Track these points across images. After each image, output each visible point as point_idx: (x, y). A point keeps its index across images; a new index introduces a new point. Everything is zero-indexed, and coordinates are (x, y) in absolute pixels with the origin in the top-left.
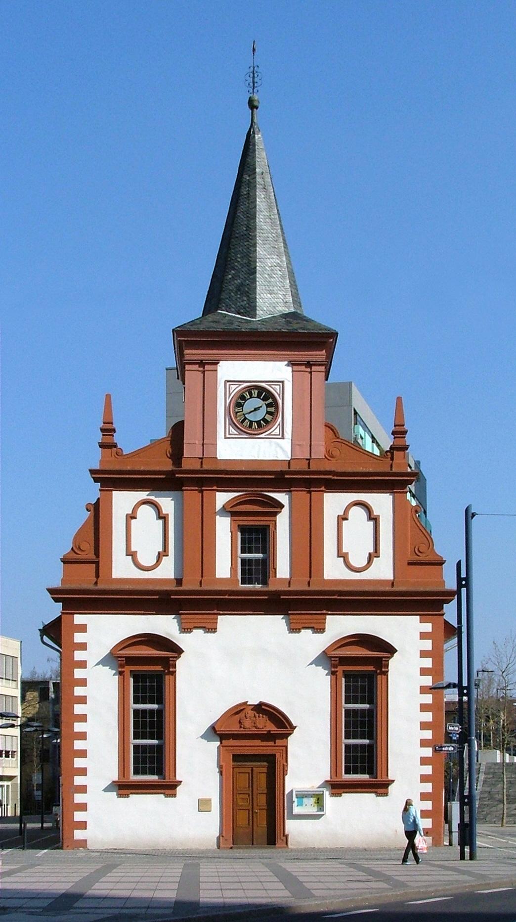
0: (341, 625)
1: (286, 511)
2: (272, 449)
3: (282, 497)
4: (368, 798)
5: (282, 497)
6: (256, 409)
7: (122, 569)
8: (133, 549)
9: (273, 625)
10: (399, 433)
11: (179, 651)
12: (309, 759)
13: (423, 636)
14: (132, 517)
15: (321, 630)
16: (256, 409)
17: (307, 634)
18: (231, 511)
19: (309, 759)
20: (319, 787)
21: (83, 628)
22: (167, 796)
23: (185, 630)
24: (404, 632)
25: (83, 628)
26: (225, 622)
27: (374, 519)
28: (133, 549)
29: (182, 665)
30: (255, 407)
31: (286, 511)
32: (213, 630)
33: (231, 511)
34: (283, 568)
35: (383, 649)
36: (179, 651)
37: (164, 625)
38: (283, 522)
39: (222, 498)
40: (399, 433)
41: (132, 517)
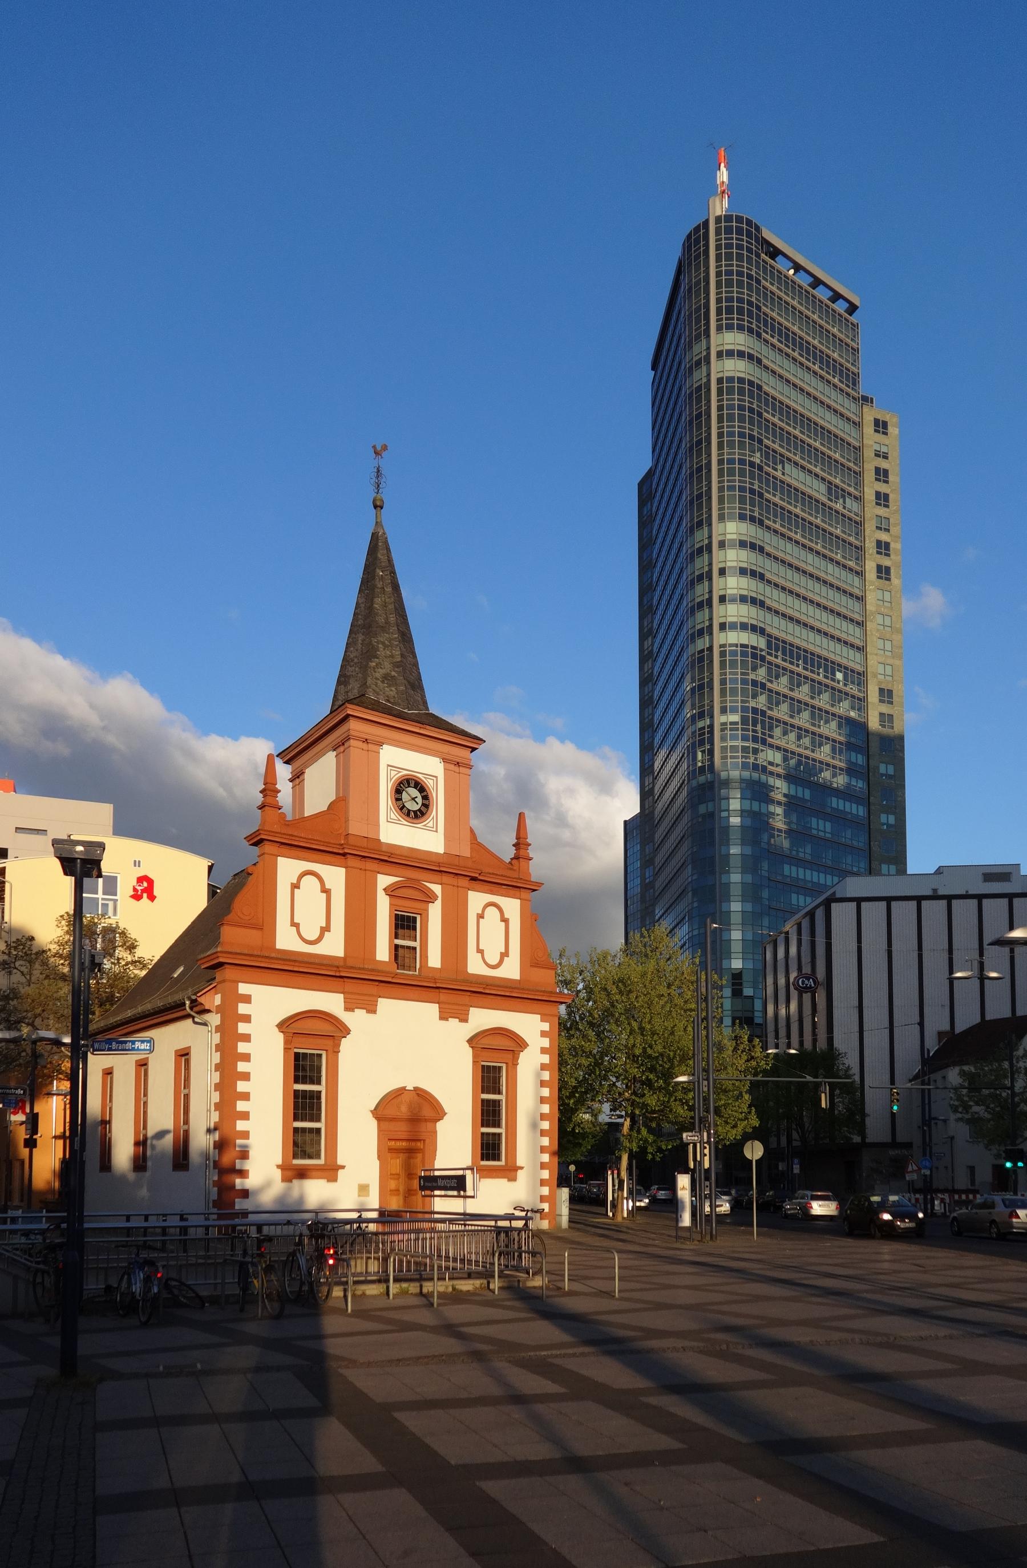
0: (484, 1018)
1: (438, 903)
2: (428, 839)
3: (437, 889)
4: (502, 1183)
5: (437, 889)
6: (412, 798)
7: (286, 940)
8: (327, 887)
9: (424, 1013)
10: (521, 844)
11: (345, 1031)
12: (453, 1146)
13: (543, 1034)
14: (295, 886)
15: (466, 1020)
16: (412, 798)
17: (454, 1022)
18: (390, 891)
19: (453, 1146)
20: (939, 1042)
21: (247, 999)
22: (509, 1180)
23: (348, 1008)
24: (532, 1028)
25: (247, 999)
26: (384, 1004)
27: (505, 920)
28: (324, 895)
29: (345, 1044)
30: (411, 798)
31: (438, 903)
32: (372, 1010)
33: (390, 891)
34: (435, 960)
35: (515, 1044)
36: (345, 1031)
37: (331, 1002)
38: (435, 912)
39: (384, 881)
40: (521, 844)
41: (295, 886)
